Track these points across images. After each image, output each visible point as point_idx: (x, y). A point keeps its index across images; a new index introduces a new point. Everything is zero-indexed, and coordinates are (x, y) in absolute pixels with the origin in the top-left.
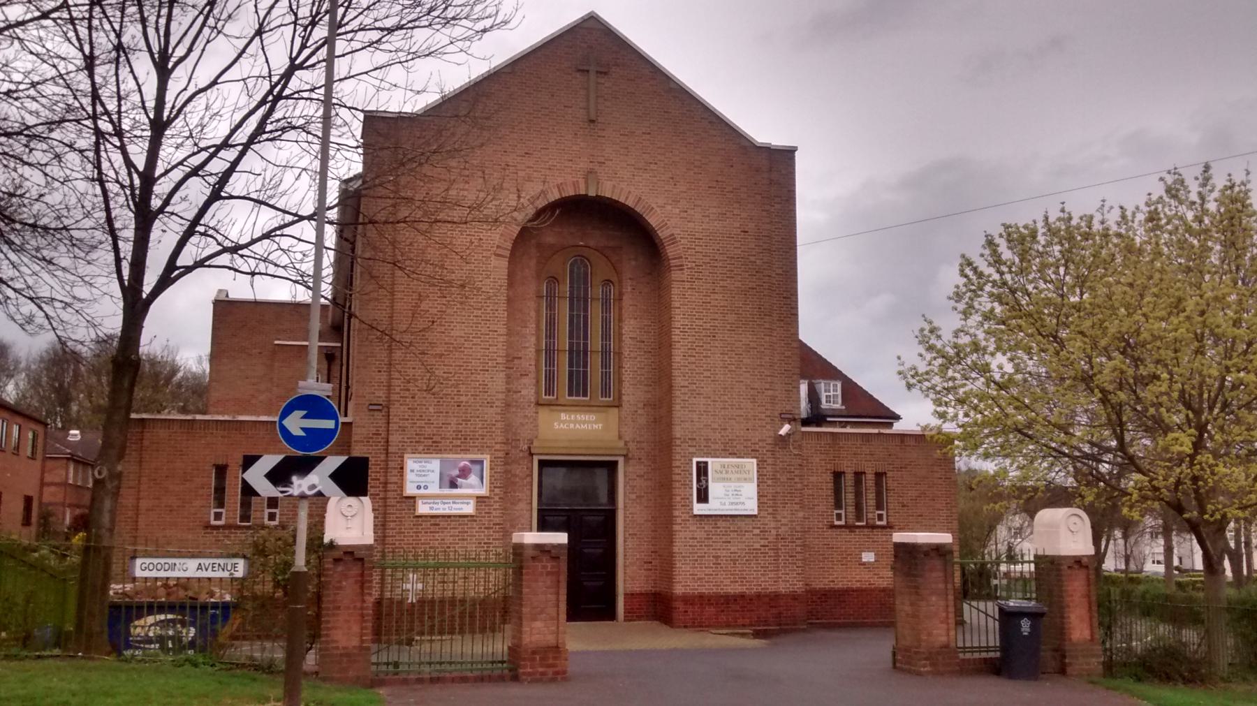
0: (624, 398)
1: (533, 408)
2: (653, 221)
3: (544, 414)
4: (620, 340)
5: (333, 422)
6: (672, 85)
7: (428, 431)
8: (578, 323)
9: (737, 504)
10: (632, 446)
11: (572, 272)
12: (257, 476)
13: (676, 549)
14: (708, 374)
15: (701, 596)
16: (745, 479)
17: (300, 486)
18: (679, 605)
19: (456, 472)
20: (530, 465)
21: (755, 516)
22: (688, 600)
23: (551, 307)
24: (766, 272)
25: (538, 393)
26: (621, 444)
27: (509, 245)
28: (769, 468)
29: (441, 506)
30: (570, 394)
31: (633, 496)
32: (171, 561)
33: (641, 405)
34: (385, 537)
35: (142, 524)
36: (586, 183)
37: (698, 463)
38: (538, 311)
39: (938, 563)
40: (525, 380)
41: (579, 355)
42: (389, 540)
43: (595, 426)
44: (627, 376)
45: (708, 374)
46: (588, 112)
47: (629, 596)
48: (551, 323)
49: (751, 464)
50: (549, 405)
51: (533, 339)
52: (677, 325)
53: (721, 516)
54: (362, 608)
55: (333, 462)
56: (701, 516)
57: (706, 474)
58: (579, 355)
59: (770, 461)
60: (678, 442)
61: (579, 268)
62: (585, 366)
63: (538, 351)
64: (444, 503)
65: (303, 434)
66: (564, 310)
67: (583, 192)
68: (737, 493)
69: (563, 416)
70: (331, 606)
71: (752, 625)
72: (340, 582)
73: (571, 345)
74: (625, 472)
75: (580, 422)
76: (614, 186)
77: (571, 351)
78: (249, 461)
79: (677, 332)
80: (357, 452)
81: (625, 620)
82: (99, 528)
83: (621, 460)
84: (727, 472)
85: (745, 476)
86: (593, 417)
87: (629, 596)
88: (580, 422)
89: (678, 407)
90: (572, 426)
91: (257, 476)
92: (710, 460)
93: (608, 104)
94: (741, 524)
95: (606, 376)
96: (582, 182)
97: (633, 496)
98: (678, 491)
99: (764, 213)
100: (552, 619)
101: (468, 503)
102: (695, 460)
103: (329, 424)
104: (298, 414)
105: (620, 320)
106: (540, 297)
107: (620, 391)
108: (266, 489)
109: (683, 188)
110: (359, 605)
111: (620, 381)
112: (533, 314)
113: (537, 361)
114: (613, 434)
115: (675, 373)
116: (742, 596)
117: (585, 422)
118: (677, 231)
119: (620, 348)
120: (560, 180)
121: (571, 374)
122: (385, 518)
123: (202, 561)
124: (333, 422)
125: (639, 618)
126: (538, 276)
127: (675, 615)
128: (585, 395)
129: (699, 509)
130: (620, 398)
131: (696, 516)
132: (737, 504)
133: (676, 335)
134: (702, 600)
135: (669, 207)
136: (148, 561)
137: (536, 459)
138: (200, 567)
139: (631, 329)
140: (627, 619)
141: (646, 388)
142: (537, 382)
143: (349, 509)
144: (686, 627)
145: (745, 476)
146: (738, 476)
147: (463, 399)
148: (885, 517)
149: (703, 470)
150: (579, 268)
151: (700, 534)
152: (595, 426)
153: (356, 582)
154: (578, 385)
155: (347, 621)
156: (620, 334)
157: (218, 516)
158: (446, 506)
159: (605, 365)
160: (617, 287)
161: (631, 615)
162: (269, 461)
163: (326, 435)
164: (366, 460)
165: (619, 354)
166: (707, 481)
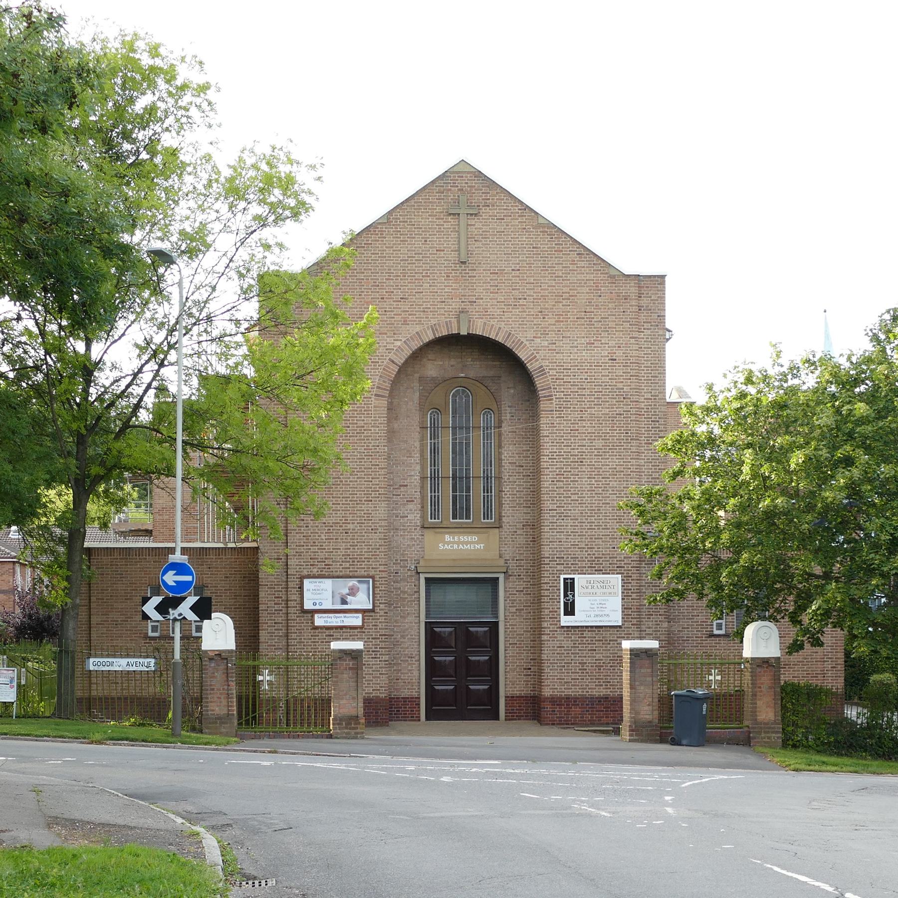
0: (504, 519)
1: (417, 534)
2: (522, 355)
3: (429, 535)
4: (500, 466)
5: (191, 577)
6: (541, 221)
7: (321, 555)
8: (461, 451)
9: (601, 616)
10: (512, 564)
11: (454, 402)
12: (150, 608)
13: (544, 657)
14: (576, 497)
15: (568, 698)
16: (610, 593)
17: (173, 614)
18: (548, 707)
19: (346, 591)
20: (417, 583)
21: (620, 627)
22: (555, 701)
23: (434, 436)
24: (635, 398)
25: (423, 517)
26: (501, 562)
27: (388, 385)
28: (634, 583)
29: (334, 620)
30: (454, 517)
31: (514, 610)
32: (110, 660)
33: (520, 526)
34: (288, 645)
35: (94, 636)
36: (459, 322)
37: (565, 579)
38: (422, 439)
39: (647, 662)
40: (411, 506)
41: (461, 481)
42: (291, 648)
43: (477, 546)
44: (507, 499)
45: (576, 497)
46: (459, 254)
47: (510, 699)
48: (434, 451)
49: (616, 580)
50: (433, 527)
51: (418, 467)
52: (546, 452)
53: (587, 627)
54: (228, 690)
55: (192, 600)
56: (568, 627)
57: (573, 590)
58: (461, 481)
59: (634, 577)
60: (547, 561)
61: (461, 398)
62: (468, 490)
63: (423, 478)
64: (337, 617)
65: (174, 584)
66: (447, 439)
67: (455, 332)
68: (602, 606)
69: (448, 538)
70: (209, 688)
71: (612, 724)
72: (214, 673)
73: (454, 472)
74: (505, 588)
75: (463, 543)
76: (485, 323)
77: (454, 478)
78: (145, 600)
79: (546, 459)
80: (207, 594)
81: (506, 720)
82: (67, 639)
83: (501, 577)
84: (592, 587)
85: (610, 590)
86: (475, 538)
87: (510, 699)
88: (463, 543)
89: (546, 529)
90: (455, 546)
91: (150, 608)
92: (576, 577)
93: (479, 244)
94: (607, 634)
95: (487, 501)
96: (454, 321)
97: (514, 610)
98: (547, 606)
99: (632, 341)
100: (353, 698)
101: (357, 617)
102: (562, 577)
103: (188, 578)
104: (171, 573)
105: (500, 446)
106: (424, 428)
107: (500, 513)
108: (155, 616)
109: (552, 321)
110: (226, 687)
111: (500, 505)
112: (417, 444)
113: (422, 487)
114: (494, 554)
115: (545, 497)
116: (606, 698)
117: (467, 543)
118: (545, 363)
119: (500, 472)
120: (433, 322)
121: (455, 498)
122: (287, 630)
123: (129, 660)
124: (191, 577)
125: (519, 718)
126: (422, 409)
127: (544, 714)
128: (468, 517)
129: (566, 621)
130: (500, 519)
131: (563, 627)
132: (601, 616)
133: (545, 462)
134: (570, 702)
135: (539, 340)
136: (97, 660)
137: (422, 577)
138: (128, 664)
139: (510, 453)
140: (507, 719)
141: (525, 510)
142: (423, 507)
143: (217, 627)
144: (553, 724)
145: (610, 590)
146: (605, 590)
147: (351, 526)
148: (724, 627)
149: (570, 586)
150: (461, 398)
151: (567, 644)
152: (477, 546)
153: (224, 673)
154: (461, 509)
155: (219, 698)
156: (500, 460)
157: (719, 627)
158: (338, 620)
159: (487, 489)
160: (497, 415)
161: (511, 716)
162: (156, 600)
163: (187, 585)
164: (210, 598)
165: (499, 478)
166: (574, 596)
